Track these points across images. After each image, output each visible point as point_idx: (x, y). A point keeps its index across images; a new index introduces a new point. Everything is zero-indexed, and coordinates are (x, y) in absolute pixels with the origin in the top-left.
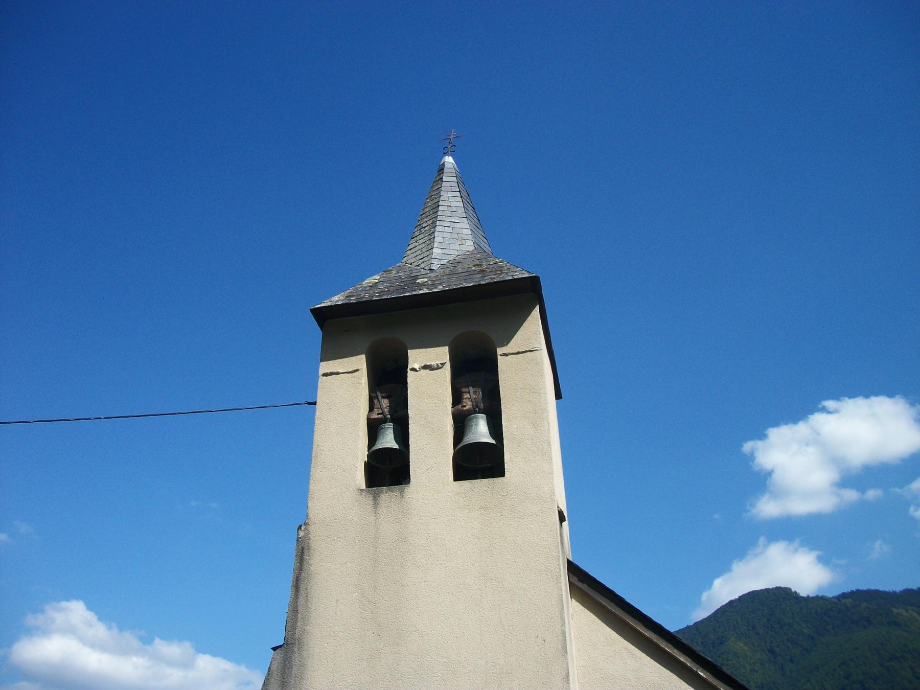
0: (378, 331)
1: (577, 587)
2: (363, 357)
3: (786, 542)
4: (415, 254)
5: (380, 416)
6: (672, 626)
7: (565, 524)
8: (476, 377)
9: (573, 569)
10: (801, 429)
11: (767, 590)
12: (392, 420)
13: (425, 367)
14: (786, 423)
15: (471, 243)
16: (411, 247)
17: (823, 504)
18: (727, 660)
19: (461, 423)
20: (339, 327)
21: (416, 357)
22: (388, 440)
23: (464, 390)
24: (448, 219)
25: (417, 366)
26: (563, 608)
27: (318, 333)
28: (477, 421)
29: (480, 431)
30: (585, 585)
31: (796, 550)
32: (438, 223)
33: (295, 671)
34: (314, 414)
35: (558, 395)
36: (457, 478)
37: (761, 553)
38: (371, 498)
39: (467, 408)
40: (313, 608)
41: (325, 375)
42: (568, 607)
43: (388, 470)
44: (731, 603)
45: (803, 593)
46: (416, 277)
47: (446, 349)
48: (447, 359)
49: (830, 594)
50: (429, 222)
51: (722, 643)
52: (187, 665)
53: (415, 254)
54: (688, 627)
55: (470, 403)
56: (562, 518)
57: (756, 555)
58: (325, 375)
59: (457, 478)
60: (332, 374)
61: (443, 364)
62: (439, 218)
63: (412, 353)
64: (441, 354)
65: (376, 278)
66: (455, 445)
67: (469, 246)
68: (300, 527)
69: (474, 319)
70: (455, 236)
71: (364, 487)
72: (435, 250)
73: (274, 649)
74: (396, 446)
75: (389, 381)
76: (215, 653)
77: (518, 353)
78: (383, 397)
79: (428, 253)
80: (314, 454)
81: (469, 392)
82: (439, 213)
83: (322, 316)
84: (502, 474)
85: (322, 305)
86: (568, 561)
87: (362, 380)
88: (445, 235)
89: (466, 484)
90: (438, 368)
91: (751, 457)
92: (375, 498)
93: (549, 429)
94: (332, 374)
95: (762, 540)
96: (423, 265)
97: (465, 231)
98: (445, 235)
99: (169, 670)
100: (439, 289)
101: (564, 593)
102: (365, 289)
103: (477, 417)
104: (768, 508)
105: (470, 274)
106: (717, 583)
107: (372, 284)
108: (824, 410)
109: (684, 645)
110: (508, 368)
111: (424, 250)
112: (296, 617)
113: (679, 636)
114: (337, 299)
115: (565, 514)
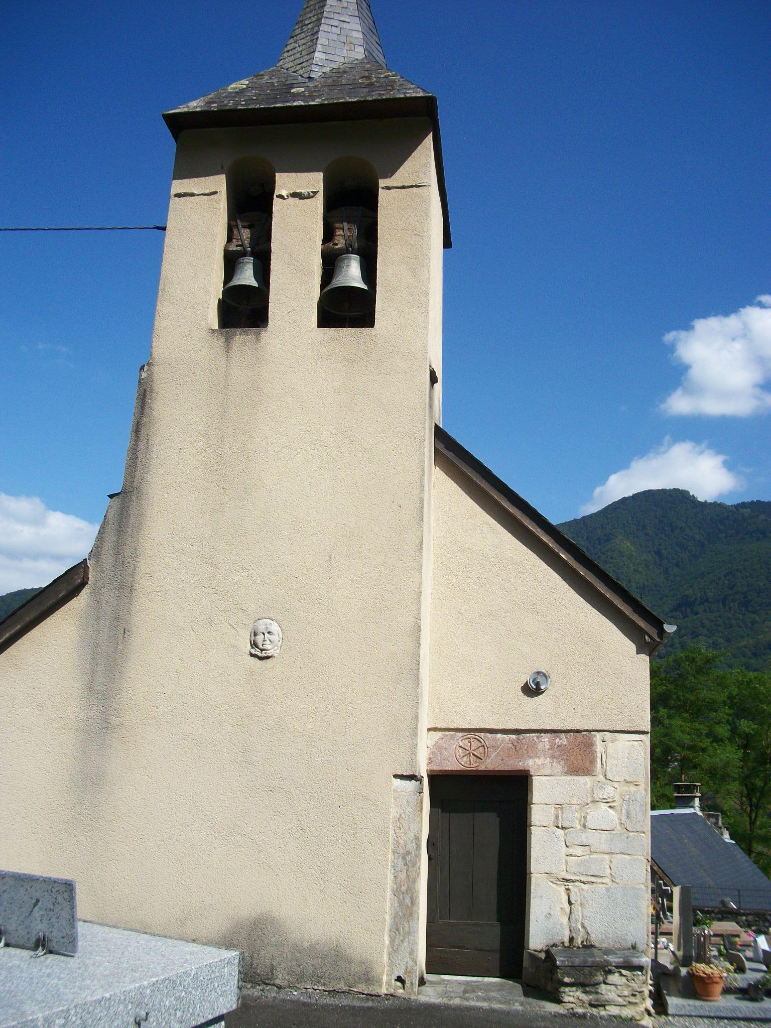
0: (243, 147)
1: (443, 455)
2: (223, 177)
3: (693, 444)
4: (292, 58)
5: (239, 248)
6: (554, 520)
7: (438, 386)
8: (352, 211)
9: (440, 434)
10: (732, 322)
11: (663, 491)
12: (253, 254)
13: (295, 195)
14: (715, 315)
15: (361, 50)
16: (289, 48)
17: (741, 406)
18: (611, 558)
19: (331, 263)
20: (199, 138)
21: (285, 183)
22: (247, 277)
23: (337, 225)
24: (336, 16)
25: (284, 193)
26: (423, 474)
27: (172, 145)
28: (349, 262)
29: (352, 274)
30: (451, 453)
31: (702, 452)
32: (323, 21)
33: (132, 520)
34: (163, 241)
35: (447, 244)
36: (320, 325)
37: (664, 453)
38: (223, 340)
39: (339, 246)
40: (154, 456)
41: (178, 195)
42: (430, 475)
43: (244, 310)
44: (624, 500)
45: (701, 499)
46: (292, 86)
47: (320, 175)
48: (320, 188)
49: (729, 502)
50: (313, 19)
51: (608, 540)
52: (37, 522)
53: (292, 58)
54: (575, 520)
55: (343, 241)
56: (433, 379)
57: (659, 454)
58: (178, 195)
59: (320, 325)
60: (185, 195)
61: (315, 193)
62: (325, 14)
63: (280, 178)
64: (313, 182)
65: (244, 83)
66: (322, 287)
67: (359, 53)
68: (142, 368)
69: (355, 142)
70: (343, 39)
71: (217, 327)
72: (317, 54)
73: (111, 496)
74: (255, 284)
75: (251, 209)
76: (67, 511)
77: (403, 187)
78: (244, 227)
79: (308, 57)
80: (161, 287)
81: (343, 229)
82: (327, 9)
83: (178, 124)
84: (373, 326)
85: (177, 111)
86: (437, 427)
87: (221, 204)
88: (331, 36)
89: (331, 332)
90: (309, 197)
91: (672, 348)
92: (228, 340)
93: (429, 279)
94: (185, 195)
95: (667, 438)
96: (301, 72)
97: (355, 34)
98: (331, 36)
99: (19, 527)
100: (317, 101)
101: (426, 459)
102: (230, 96)
103: (349, 258)
104: (680, 404)
105: (354, 87)
106: (613, 479)
107: (238, 91)
108: (762, 306)
109: (572, 545)
110: (390, 203)
111: (304, 53)
112: (135, 463)
113: (560, 530)
114: (196, 105)
115: (439, 375)
